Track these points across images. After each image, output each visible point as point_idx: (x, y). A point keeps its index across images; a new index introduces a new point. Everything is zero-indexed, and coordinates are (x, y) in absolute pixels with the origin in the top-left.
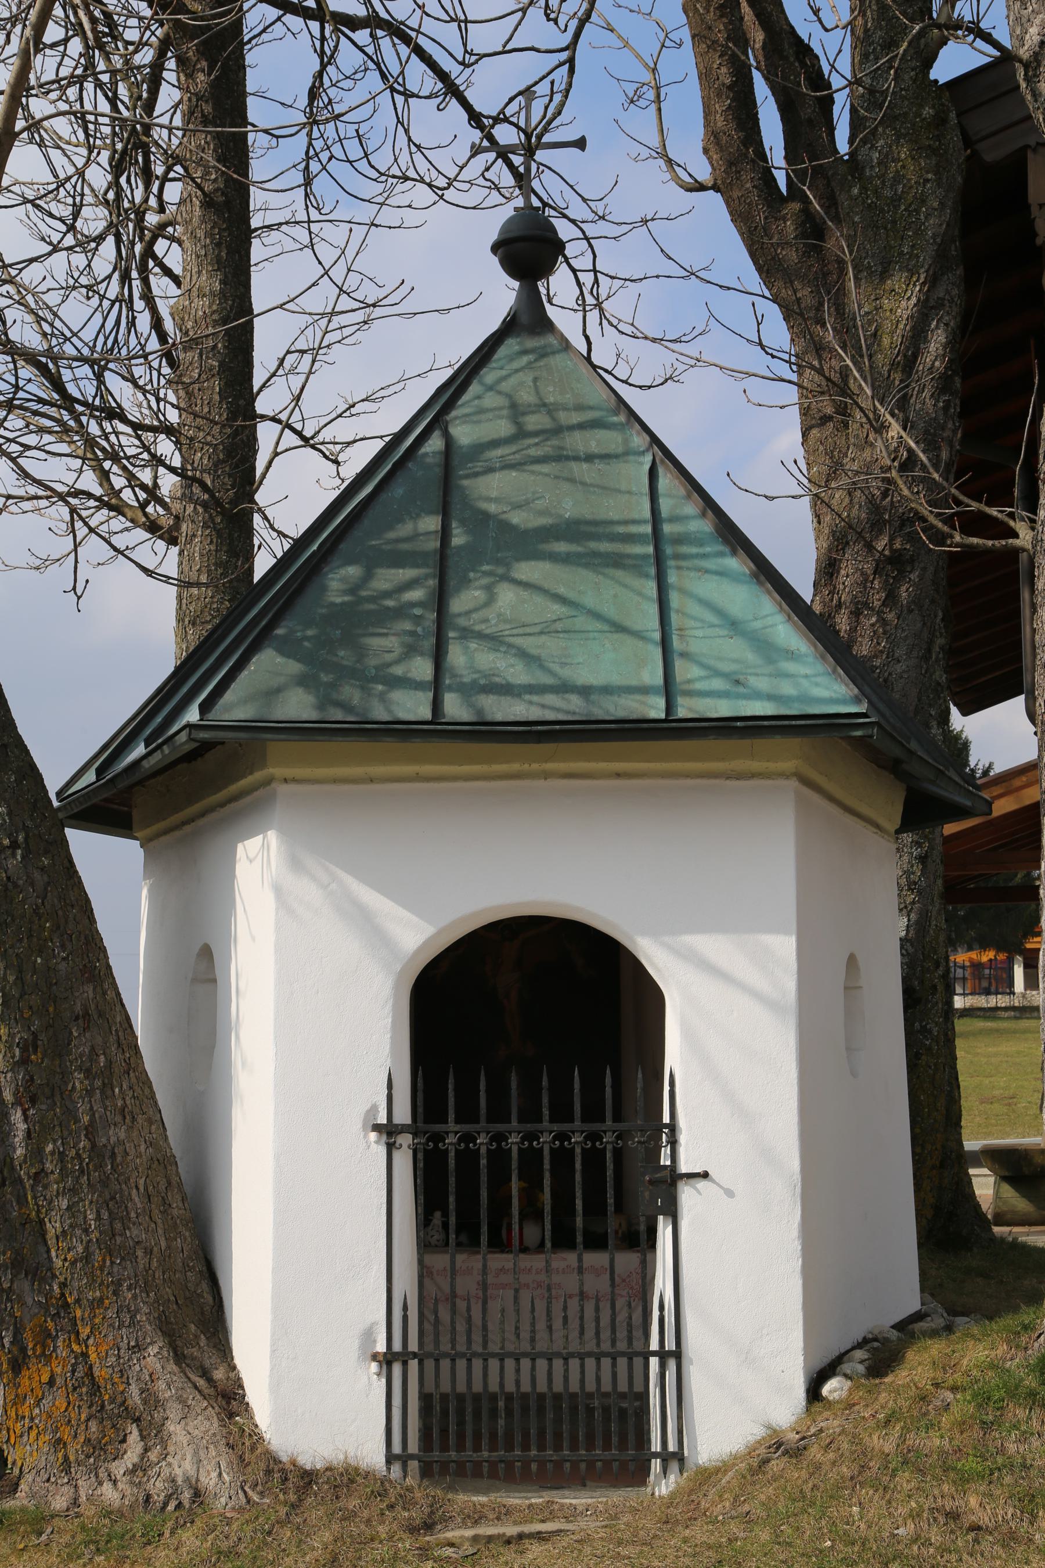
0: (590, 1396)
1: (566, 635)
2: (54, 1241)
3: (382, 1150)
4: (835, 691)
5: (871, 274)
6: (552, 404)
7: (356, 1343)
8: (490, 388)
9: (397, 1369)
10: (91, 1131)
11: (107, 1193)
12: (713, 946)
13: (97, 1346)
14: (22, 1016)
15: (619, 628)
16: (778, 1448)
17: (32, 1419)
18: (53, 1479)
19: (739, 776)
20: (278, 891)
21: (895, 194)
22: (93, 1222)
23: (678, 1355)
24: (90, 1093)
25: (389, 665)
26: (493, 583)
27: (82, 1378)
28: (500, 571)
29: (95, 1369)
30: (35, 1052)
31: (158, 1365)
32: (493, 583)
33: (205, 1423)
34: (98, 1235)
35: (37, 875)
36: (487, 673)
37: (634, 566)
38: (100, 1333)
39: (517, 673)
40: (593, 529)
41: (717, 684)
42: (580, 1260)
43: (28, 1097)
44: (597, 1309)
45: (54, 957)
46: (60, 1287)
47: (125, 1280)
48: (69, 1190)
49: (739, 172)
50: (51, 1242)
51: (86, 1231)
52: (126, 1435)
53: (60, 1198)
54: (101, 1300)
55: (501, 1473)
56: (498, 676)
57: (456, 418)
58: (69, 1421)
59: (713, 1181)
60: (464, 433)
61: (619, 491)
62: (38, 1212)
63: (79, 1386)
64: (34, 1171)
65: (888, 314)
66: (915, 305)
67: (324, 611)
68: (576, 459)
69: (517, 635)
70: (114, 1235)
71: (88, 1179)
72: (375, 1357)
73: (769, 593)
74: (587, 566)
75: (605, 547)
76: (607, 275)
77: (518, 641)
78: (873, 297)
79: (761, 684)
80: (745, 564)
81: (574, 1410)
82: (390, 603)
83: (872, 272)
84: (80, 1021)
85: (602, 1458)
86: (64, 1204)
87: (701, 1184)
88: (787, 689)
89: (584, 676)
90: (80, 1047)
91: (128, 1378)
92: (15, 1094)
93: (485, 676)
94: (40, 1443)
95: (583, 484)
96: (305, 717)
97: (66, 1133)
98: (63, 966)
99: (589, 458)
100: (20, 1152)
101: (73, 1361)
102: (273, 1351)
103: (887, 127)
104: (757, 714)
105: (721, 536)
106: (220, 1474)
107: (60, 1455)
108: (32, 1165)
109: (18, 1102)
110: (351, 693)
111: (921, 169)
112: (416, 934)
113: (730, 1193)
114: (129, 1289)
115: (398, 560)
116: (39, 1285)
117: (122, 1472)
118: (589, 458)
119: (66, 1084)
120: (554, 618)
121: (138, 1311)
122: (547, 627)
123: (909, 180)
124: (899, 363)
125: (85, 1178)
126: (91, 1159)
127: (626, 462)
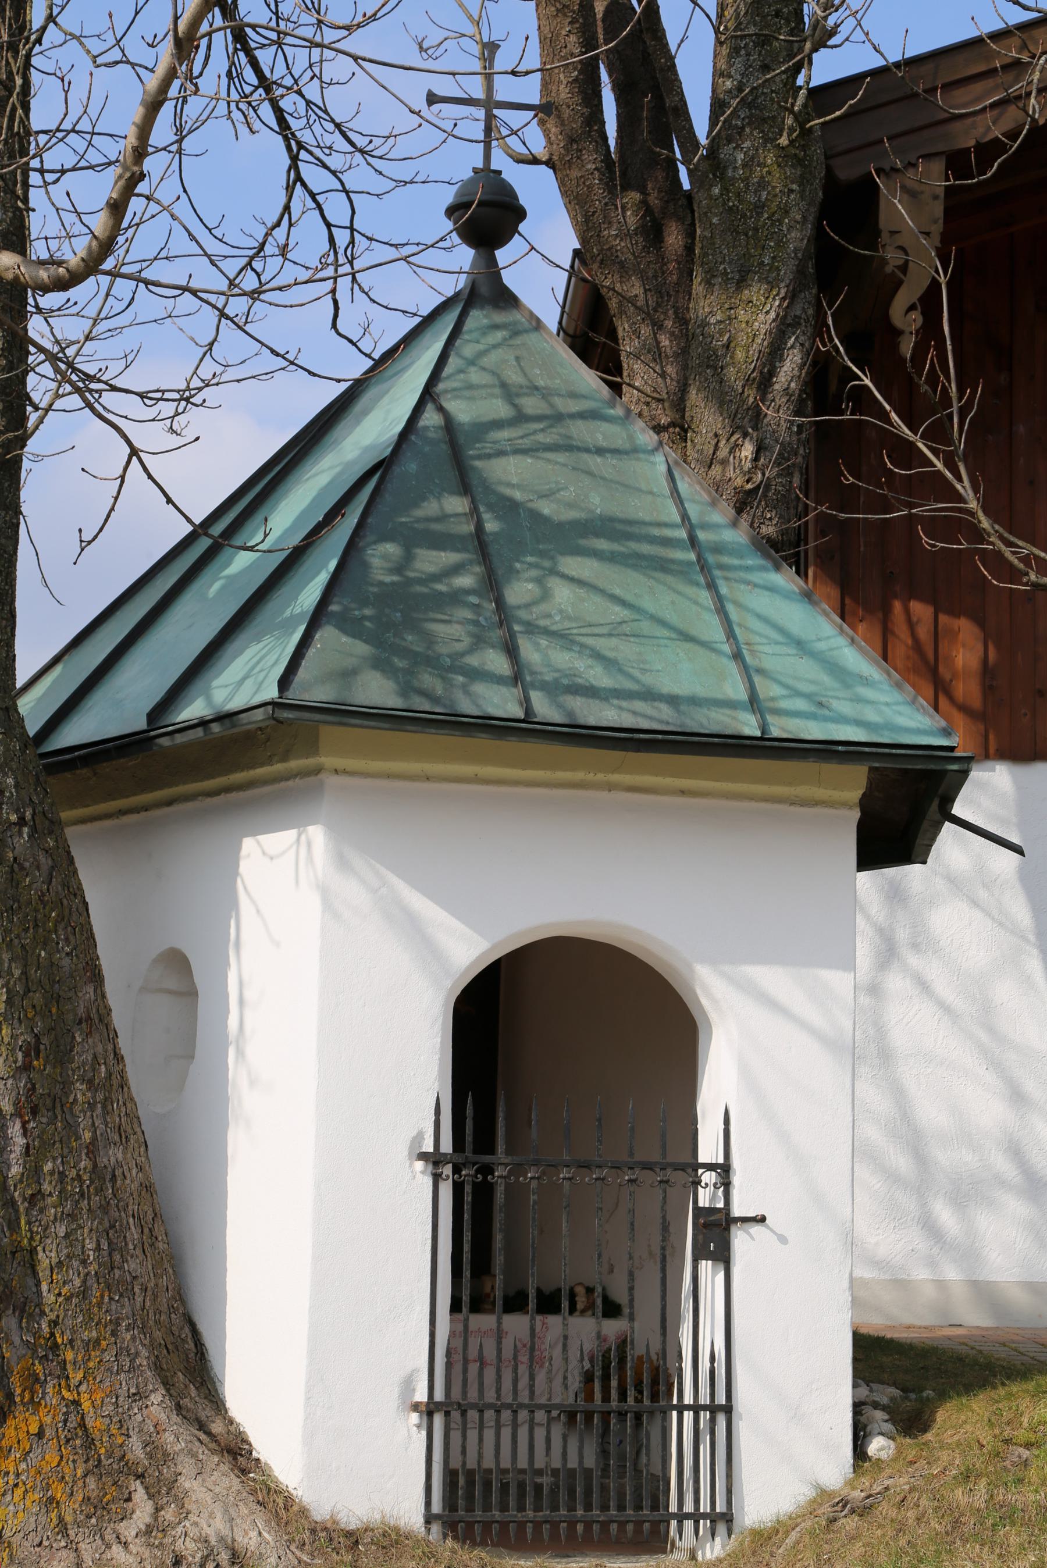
0: (506, 1471)
1: (637, 640)
2: (48, 1272)
3: (428, 1181)
4: (920, 722)
5: (727, 281)
6: (544, 388)
7: (396, 1391)
8: (472, 363)
9: (438, 1420)
10: (92, 1150)
11: (106, 1220)
12: (772, 978)
13: (91, 1393)
14: (26, 1015)
15: (687, 637)
16: (844, 1506)
17: (18, 1475)
18: (46, 1543)
19: (805, 803)
20: (325, 893)
21: (759, 200)
22: (91, 1253)
23: (728, 1409)
24: (92, 1106)
25: (463, 654)
26: (544, 576)
27: (75, 1429)
28: (547, 564)
29: (87, 1420)
30: (37, 1057)
31: (163, 1415)
32: (544, 576)
33: (223, 1479)
34: (97, 1267)
35: (42, 858)
36: (568, 672)
37: (682, 572)
38: (95, 1379)
39: (598, 676)
40: (629, 529)
41: (800, 704)
42: (499, 1323)
43: (29, 1108)
44: (499, 1377)
45: (58, 951)
46: (50, 1326)
47: (123, 1319)
48: (68, 1215)
49: (581, 151)
50: (43, 1272)
51: (84, 1262)
52: (130, 1493)
53: (58, 1224)
54: (98, 1341)
55: (546, 1536)
56: (581, 677)
57: (446, 391)
58: (63, 1477)
59: (768, 1227)
60: (463, 411)
61: (639, 490)
62: (32, 1239)
63: (72, 1438)
64: (30, 1192)
65: (744, 325)
66: (774, 320)
67: (375, 590)
68: (587, 450)
69: (587, 635)
70: (112, 1269)
71: (89, 1204)
72: (416, 1407)
73: (826, 615)
74: (635, 567)
75: (645, 548)
76: (363, 235)
77: (590, 641)
78: (727, 306)
79: (844, 708)
80: (793, 582)
81: (487, 1485)
82: (441, 587)
83: (728, 279)
84: (84, 1025)
85: (650, 1518)
86: (62, 1231)
87: (755, 1229)
88: (871, 715)
89: (667, 686)
90: (82, 1056)
91: (128, 1429)
92: (16, 1104)
93: (566, 676)
94: (28, 1503)
95: (603, 478)
96: (390, 704)
97: (66, 1151)
98: (66, 962)
99: (600, 451)
100: (15, 1170)
101: (65, 1410)
102: (308, 1399)
103: (755, 129)
104: (851, 739)
105: (759, 550)
106: (260, 1533)
107: (53, 1515)
108: (28, 1185)
109: (18, 1113)
110: (428, 680)
111: (786, 178)
112: (467, 950)
113: (783, 1239)
114: (127, 1330)
115: (440, 542)
116: (27, 1322)
117: (134, 1533)
118: (600, 451)
119: (67, 1095)
120: (619, 620)
121: (137, 1354)
122: (615, 628)
123: (774, 188)
124: (754, 379)
125: (86, 1202)
126: (92, 1182)
127: (638, 459)
